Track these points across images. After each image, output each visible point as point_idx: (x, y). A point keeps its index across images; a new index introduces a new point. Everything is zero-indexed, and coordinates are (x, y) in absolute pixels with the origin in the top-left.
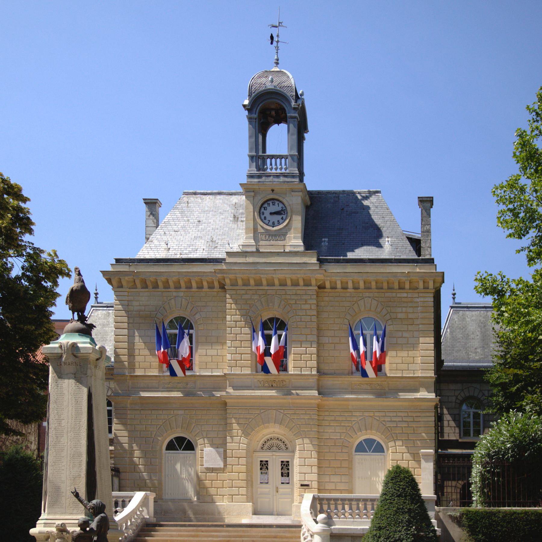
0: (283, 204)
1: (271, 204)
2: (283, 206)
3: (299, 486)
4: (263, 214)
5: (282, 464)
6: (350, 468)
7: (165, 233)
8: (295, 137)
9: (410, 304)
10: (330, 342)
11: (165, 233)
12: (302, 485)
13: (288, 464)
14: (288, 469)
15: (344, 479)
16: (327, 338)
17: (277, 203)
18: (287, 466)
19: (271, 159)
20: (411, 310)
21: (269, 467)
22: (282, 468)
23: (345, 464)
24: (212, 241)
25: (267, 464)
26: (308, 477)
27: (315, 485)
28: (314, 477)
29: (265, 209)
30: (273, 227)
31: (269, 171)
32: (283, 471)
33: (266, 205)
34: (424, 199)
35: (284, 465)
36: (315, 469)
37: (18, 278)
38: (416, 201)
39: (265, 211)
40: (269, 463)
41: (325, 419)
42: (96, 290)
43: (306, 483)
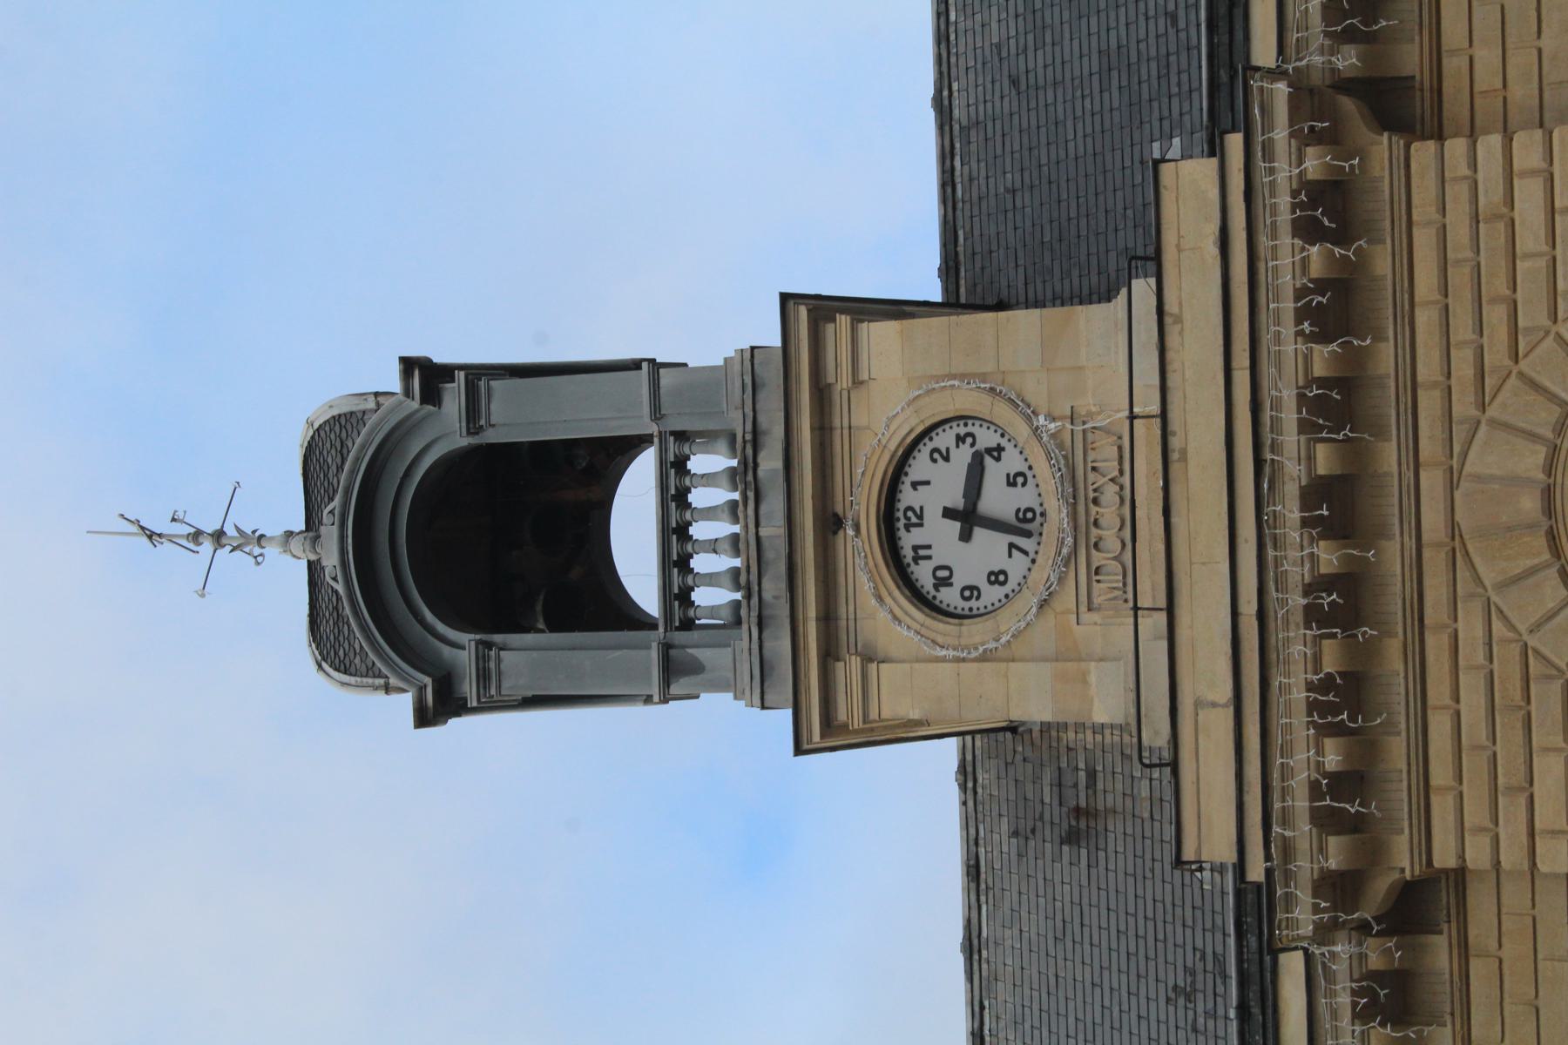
4: (971, 591)
33: (923, 574)
39: (959, 581)
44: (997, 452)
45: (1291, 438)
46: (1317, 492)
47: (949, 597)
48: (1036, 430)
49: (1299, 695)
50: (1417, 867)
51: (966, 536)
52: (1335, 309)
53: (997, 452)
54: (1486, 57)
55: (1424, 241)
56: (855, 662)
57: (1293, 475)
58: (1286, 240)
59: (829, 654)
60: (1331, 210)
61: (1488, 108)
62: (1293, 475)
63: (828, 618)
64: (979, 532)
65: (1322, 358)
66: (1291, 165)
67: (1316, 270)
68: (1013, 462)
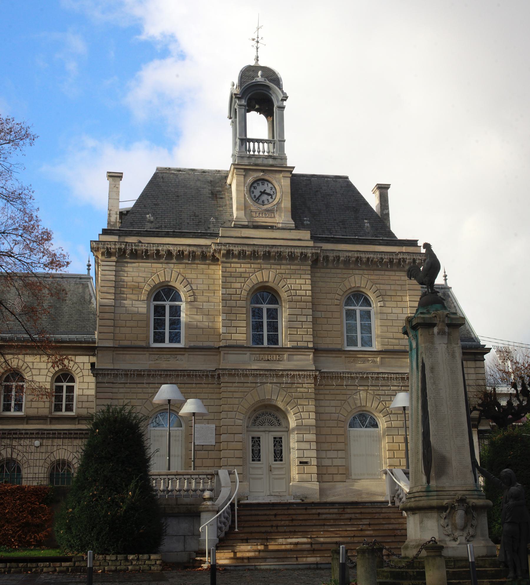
0: (272, 184)
1: (261, 184)
2: (272, 186)
3: (297, 462)
4: (253, 192)
5: (274, 441)
6: (346, 443)
7: (145, 206)
8: (271, 126)
9: (398, 282)
10: (323, 317)
11: (145, 206)
12: (301, 463)
13: (281, 441)
14: (281, 446)
15: (341, 454)
16: (320, 313)
17: (266, 183)
18: (279, 443)
19: (249, 142)
20: (399, 288)
21: (261, 444)
22: (275, 446)
23: (341, 439)
24: (194, 215)
25: (259, 441)
26: (307, 454)
27: (314, 462)
28: (314, 454)
29: (254, 188)
30: (263, 205)
31: (252, 153)
32: (275, 448)
33: (255, 185)
34: (382, 186)
35: (277, 441)
36: (314, 446)
37: (116, 258)
38: (105, 175)
39: (254, 190)
40: (261, 439)
41: (320, 393)
42: (89, 261)
43: (305, 460)
44: (272, 198)
45: (276, 250)
46: (244, 252)
47: (252, 189)
48: (275, 205)
49: (244, 249)
50: (353, 279)
51: (261, 192)
52: (292, 257)
53: (272, 198)
54: (319, 275)
55: (298, 267)
56: (244, 174)
57: (363, 255)
58: (300, 251)
59: (245, 170)
60: (304, 257)
61: (119, 269)
62: (363, 255)
63: (250, 169)
64: (260, 194)
65: (236, 253)
66: (309, 252)
67: (235, 252)
68: (271, 200)
